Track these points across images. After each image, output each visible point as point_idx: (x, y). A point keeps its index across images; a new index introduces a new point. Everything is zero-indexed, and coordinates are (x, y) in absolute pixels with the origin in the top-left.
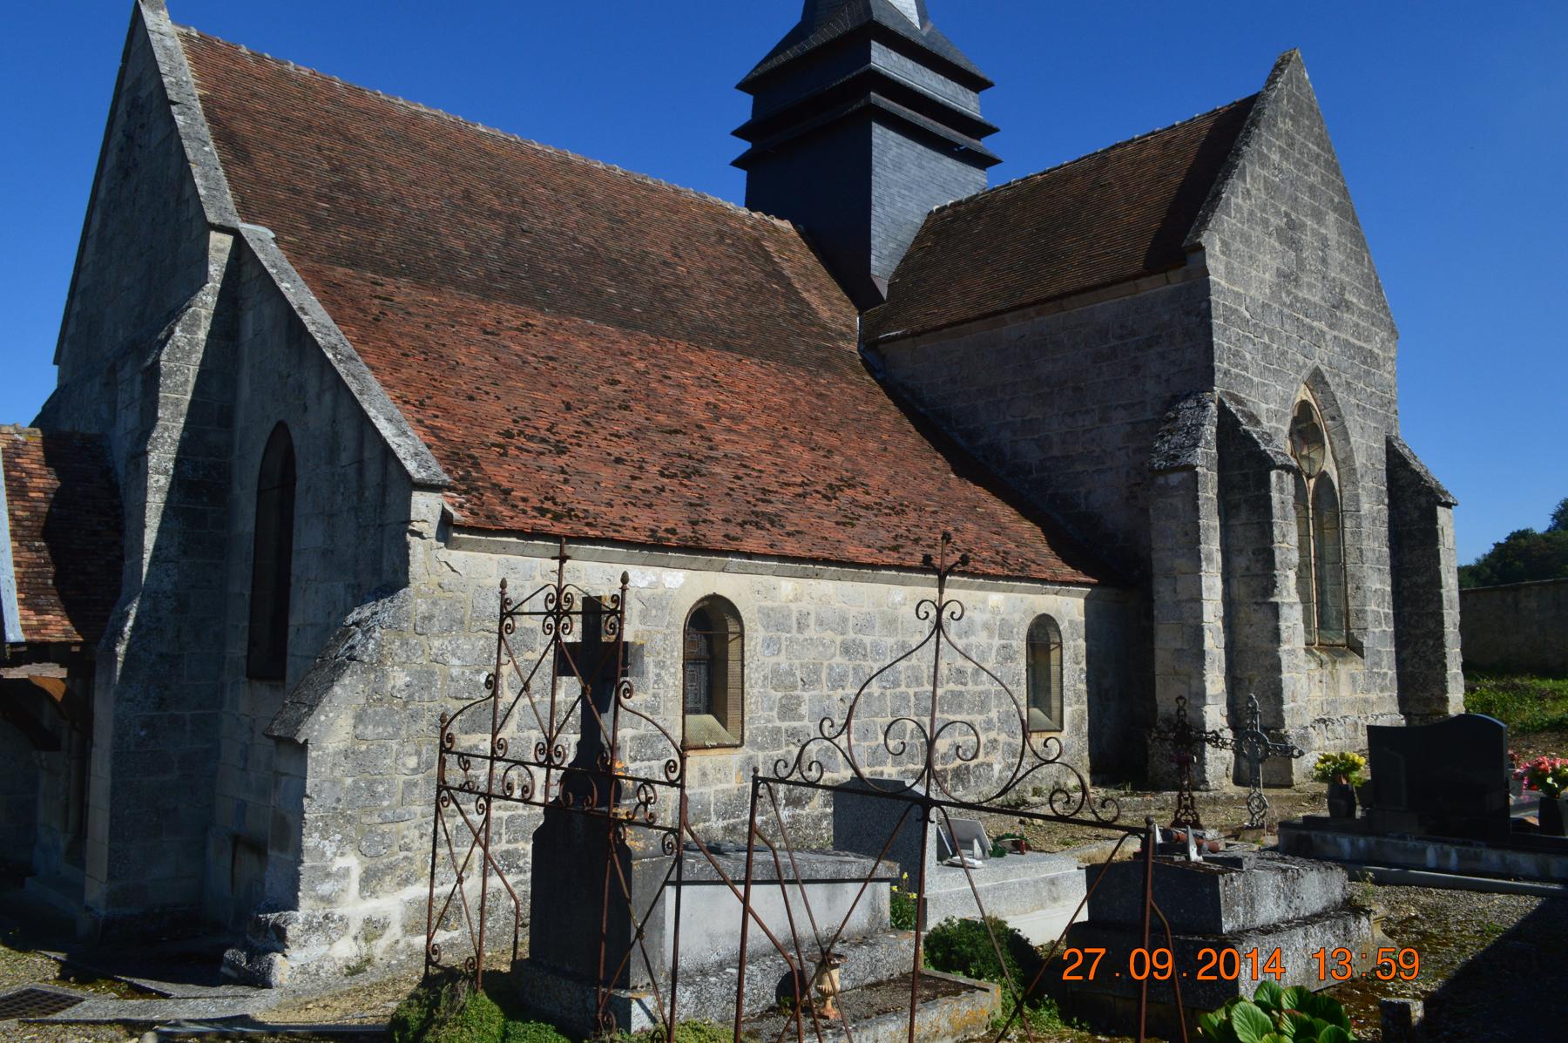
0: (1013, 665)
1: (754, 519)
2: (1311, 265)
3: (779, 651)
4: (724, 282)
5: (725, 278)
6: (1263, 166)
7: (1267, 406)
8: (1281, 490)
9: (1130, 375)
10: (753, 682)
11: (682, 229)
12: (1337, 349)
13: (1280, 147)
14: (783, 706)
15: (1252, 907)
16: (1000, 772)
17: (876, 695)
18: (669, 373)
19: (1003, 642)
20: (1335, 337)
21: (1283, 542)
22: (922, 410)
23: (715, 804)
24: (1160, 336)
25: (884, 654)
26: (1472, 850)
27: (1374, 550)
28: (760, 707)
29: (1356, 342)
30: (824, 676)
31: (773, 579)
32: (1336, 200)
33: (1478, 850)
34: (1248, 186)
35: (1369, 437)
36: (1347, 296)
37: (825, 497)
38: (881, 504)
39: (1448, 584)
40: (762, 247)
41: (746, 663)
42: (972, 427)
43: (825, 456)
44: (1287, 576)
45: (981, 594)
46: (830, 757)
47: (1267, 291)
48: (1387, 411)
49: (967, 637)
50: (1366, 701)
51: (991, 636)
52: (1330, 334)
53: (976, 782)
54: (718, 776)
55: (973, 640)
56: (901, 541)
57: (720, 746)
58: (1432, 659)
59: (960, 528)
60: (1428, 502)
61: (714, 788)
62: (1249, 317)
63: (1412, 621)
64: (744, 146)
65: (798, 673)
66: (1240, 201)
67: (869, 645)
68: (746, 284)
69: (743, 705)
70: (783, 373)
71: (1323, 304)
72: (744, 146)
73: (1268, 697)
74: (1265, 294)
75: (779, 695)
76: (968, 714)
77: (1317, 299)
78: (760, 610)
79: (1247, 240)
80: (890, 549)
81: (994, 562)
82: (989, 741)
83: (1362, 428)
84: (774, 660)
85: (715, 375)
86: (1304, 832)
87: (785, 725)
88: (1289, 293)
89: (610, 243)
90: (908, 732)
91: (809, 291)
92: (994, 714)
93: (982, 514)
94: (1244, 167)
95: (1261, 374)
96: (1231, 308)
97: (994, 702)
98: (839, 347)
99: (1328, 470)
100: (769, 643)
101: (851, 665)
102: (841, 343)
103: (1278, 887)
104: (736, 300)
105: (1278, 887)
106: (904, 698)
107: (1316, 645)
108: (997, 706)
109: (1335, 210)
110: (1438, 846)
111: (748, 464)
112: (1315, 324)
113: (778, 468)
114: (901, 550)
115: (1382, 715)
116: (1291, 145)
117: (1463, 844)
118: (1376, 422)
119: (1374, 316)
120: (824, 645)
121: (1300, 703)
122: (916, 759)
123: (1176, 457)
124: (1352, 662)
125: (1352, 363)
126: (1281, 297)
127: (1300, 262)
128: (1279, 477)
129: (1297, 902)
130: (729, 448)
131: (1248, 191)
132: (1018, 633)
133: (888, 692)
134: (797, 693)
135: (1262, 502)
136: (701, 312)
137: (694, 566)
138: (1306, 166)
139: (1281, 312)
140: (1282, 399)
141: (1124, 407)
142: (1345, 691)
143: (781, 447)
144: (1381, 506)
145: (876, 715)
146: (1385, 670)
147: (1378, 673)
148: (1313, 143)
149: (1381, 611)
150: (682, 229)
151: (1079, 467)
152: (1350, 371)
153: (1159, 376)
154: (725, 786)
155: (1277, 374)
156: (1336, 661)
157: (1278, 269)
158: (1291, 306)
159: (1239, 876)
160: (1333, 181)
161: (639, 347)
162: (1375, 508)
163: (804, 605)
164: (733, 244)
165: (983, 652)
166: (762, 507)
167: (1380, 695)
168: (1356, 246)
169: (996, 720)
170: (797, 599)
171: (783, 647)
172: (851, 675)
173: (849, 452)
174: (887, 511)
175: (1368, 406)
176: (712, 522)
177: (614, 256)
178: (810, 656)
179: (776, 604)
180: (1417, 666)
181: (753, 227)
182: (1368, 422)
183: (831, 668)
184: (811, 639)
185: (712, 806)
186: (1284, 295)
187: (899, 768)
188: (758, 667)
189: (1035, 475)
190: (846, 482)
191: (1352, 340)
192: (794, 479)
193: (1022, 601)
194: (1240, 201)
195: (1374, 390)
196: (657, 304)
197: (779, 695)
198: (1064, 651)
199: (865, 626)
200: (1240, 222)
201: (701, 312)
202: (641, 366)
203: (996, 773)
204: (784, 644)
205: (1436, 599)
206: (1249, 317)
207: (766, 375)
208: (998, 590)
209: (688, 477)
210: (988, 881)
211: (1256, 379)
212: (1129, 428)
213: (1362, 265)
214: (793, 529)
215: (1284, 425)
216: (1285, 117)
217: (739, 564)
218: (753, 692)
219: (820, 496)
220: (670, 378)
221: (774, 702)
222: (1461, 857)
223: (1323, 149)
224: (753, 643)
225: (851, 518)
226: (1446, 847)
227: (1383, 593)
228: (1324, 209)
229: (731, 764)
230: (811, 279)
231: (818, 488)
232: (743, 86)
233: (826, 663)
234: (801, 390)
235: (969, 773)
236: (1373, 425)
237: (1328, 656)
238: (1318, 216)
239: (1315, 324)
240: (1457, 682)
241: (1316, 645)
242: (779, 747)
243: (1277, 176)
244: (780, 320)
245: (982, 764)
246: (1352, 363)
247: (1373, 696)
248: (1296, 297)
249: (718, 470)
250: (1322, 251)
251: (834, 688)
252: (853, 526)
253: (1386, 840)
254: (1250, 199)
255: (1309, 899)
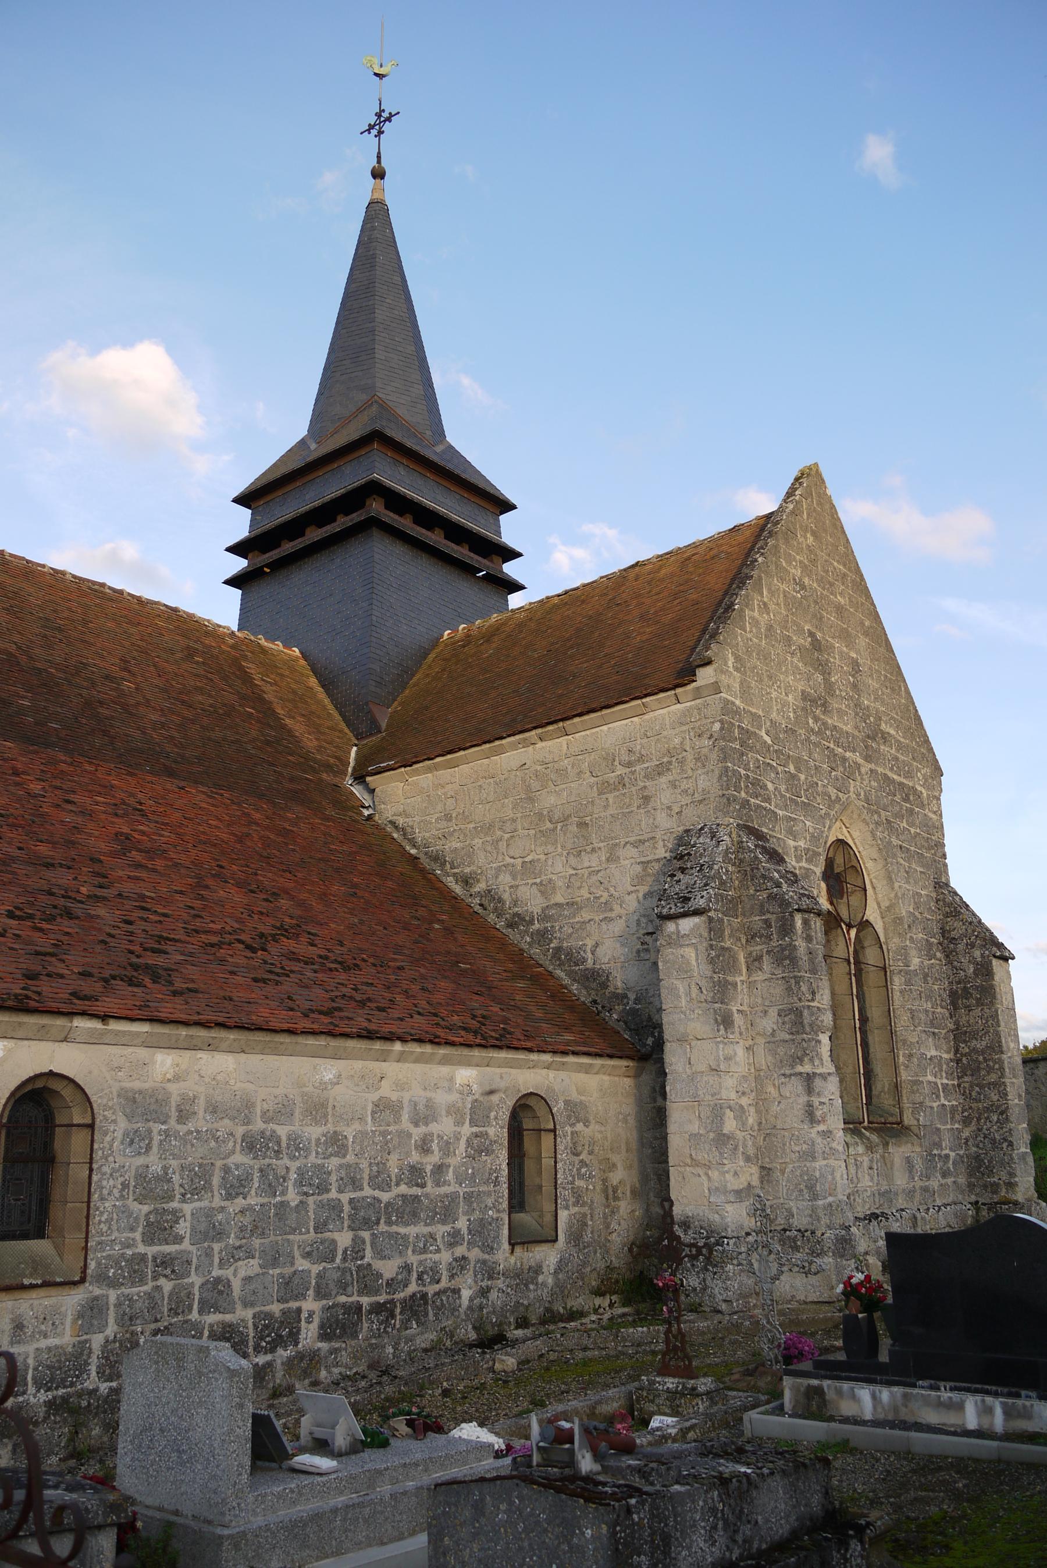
0: (489, 1159)
1: (130, 973)
2: (841, 691)
3: (149, 1148)
4: (183, 702)
5: (186, 698)
6: (782, 580)
7: (796, 844)
8: (809, 939)
9: (639, 807)
10: (105, 1192)
11: (140, 643)
12: (874, 784)
13: (801, 562)
14: (149, 1224)
15: (666, 1553)
16: (471, 1300)
17: (293, 1204)
18: (72, 797)
19: (475, 1129)
20: (871, 770)
21: (813, 1000)
22: (413, 851)
23: (35, 1369)
24: (670, 763)
25: (307, 1150)
26: (1019, 1402)
27: (927, 1011)
28: (114, 1227)
29: (895, 777)
30: (216, 1181)
31: (143, 1053)
32: (867, 623)
33: (1028, 1403)
34: (765, 600)
35: (916, 883)
36: (883, 726)
37: (249, 947)
38: (326, 958)
39: (1008, 1048)
40: (241, 668)
41: (95, 1166)
42: (467, 870)
43: (267, 900)
44: (819, 1042)
45: (445, 1070)
46: (221, 1293)
47: (791, 715)
48: (935, 854)
49: (426, 1124)
50: (925, 1189)
51: (459, 1123)
52: (866, 767)
53: (435, 1315)
54: (43, 1327)
55: (434, 1128)
56: (340, 1003)
57: (46, 1284)
58: (998, 1137)
59: (430, 987)
60: (982, 955)
61: (36, 1346)
62: (769, 742)
63: (974, 1094)
64: (239, 564)
65: (176, 1178)
66: (756, 614)
67: (284, 1139)
68: (211, 706)
69: (88, 1225)
70: (239, 804)
71: (856, 733)
72: (239, 564)
73: (801, 1191)
74: (789, 718)
75: (146, 1209)
76: (426, 1225)
77: (848, 728)
78: (123, 1093)
79: (766, 657)
80: (321, 1013)
81: (464, 1029)
82: (455, 1260)
83: (907, 872)
84: (140, 1161)
85: (141, 804)
86: (815, 1382)
87: (151, 1251)
88: (816, 719)
89: (37, 651)
90: (340, 1252)
91: (294, 718)
92: (462, 1224)
93: (465, 970)
94: (760, 578)
95: (785, 807)
96: (748, 731)
97: (462, 1207)
98: (321, 780)
99: (871, 919)
100: (131, 1139)
101: (257, 1165)
102: (324, 776)
103: (713, 1510)
104: (193, 721)
105: (713, 1510)
106: (335, 1207)
107: (866, 1124)
108: (465, 1214)
109: (866, 634)
110: (978, 1398)
111: (149, 906)
112: (848, 754)
113: (193, 912)
114: (336, 1013)
115: (945, 1205)
116: (813, 562)
117: (1010, 1395)
118: (923, 866)
119: (914, 750)
120: (217, 1140)
121: (840, 1197)
122: (349, 1289)
123: (686, 900)
124: (907, 1142)
125: (893, 800)
126: (808, 723)
127: (829, 687)
128: (806, 922)
129: (746, 1530)
130: (128, 888)
131: (765, 604)
132: (496, 1118)
133: (311, 1200)
134: (175, 1205)
135: (787, 953)
136: (144, 733)
137: (20, 1035)
138: (831, 585)
139: (808, 739)
140: (813, 836)
141: (635, 845)
142: (901, 1180)
143: (207, 887)
144: (933, 961)
145: (293, 1231)
146: (947, 1151)
147: (940, 1156)
148: (838, 562)
149: (939, 1082)
150: (140, 643)
151: (586, 915)
152: (890, 808)
153: (669, 808)
154: (52, 1342)
155: (807, 808)
156: (887, 1144)
157: (803, 692)
158: (819, 733)
159: (642, 1503)
160: (862, 604)
161: (42, 767)
162: (927, 962)
163: (189, 1086)
164: (203, 663)
165: (448, 1143)
166: (150, 959)
167: (943, 1181)
168: (891, 674)
169: (465, 1231)
170: (177, 1078)
171: (155, 1143)
172: (256, 1180)
173: (303, 896)
174: (333, 966)
175: (912, 848)
176: (62, 976)
177: (38, 665)
178: (195, 1155)
179: (146, 1086)
180: (981, 1145)
181: (233, 647)
182: (914, 866)
183: (226, 1170)
184: (198, 1132)
185: (30, 1372)
186: (811, 721)
187: (324, 1302)
188: (114, 1170)
189: (537, 926)
190: (286, 930)
191: (890, 774)
192: (211, 925)
193: (501, 1077)
194: (756, 614)
195: (918, 831)
196: (84, 721)
197: (146, 1209)
198: (559, 1140)
199: (283, 1111)
200: (757, 638)
201: (144, 733)
202: (36, 788)
203: (465, 1301)
204: (157, 1139)
205: (997, 1066)
206: (769, 742)
207: (213, 805)
208: (468, 1064)
209: (50, 919)
210: (341, 1493)
211: (780, 813)
212: (639, 868)
213: (899, 694)
214: (185, 986)
215: (816, 866)
216: (806, 531)
217: (92, 1031)
218: (105, 1207)
219: (241, 946)
220: (75, 803)
221: (137, 1219)
222: (1008, 1413)
223: (849, 570)
224: (108, 1138)
225: (277, 974)
226: (989, 1399)
227: (940, 1061)
228: (854, 632)
229: (63, 1309)
230: (300, 705)
231: (243, 937)
232: (243, 500)
233: (219, 1163)
234: (258, 824)
235: (426, 1303)
236: (919, 869)
237: (880, 1136)
238: (845, 636)
239: (848, 754)
240: (1026, 1163)
241: (866, 1124)
242: (142, 1281)
243: (799, 592)
244: (249, 747)
245: (444, 1291)
246: (893, 800)
247: (934, 1183)
248: (824, 724)
249: (102, 911)
250: (853, 676)
251: (229, 1197)
252: (277, 983)
253: (915, 1391)
254: (768, 614)
255: (767, 1521)
